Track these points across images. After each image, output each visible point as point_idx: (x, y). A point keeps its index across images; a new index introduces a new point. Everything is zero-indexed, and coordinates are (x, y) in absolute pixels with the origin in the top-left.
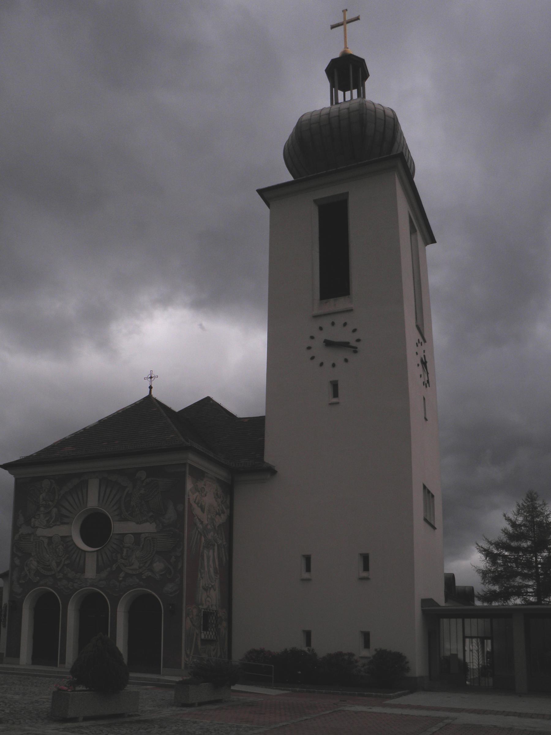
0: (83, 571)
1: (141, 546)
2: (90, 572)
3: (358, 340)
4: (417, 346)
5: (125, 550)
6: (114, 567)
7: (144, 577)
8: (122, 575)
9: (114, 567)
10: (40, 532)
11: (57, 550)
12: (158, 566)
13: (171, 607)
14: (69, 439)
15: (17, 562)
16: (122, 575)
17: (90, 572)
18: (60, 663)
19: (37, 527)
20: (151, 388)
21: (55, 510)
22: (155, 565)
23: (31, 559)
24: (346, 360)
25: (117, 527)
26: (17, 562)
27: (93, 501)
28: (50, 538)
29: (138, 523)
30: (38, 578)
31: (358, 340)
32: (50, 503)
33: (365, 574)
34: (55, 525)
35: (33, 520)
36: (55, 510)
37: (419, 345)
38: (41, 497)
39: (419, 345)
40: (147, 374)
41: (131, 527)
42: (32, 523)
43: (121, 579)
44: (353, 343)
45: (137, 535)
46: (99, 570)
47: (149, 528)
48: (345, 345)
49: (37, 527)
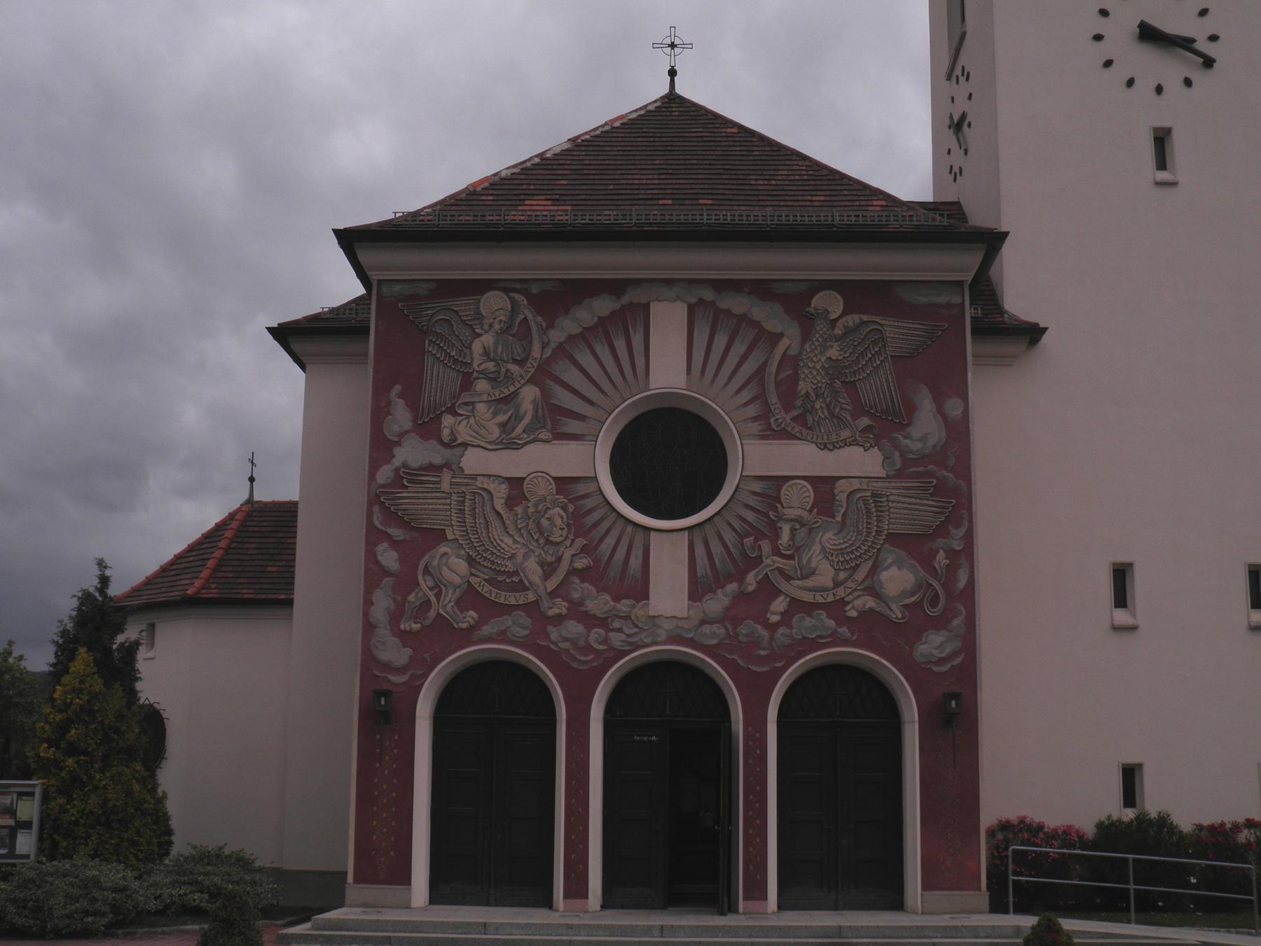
0: (641, 592)
1: (839, 519)
2: (669, 595)
3: (1213, 38)
4: (961, 169)
5: (786, 529)
6: (752, 580)
7: (855, 614)
8: (779, 604)
9: (752, 580)
10: (473, 461)
11: (544, 522)
12: (898, 578)
13: (953, 703)
14: (565, 152)
15: (389, 558)
16: (779, 604)
17: (669, 595)
18: (744, 899)
19: (465, 445)
20: (672, 73)
21: (530, 394)
22: (884, 576)
23: (443, 549)
24: (1188, 82)
25: (751, 457)
26: (389, 558)
27: (668, 367)
28: (516, 483)
29: (824, 447)
30: (472, 613)
31: (1213, 38)
32: (514, 368)
33: (1122, 617)
34: (533, 441)
35: (448, 420)
36: (530, 394)
37: (956, 169)
38: (477, 346)
39: (956, 169)
40: (663, 36)
41: (801, 458)
42: (446, 432)
43: (775, 618)
44: (1202, 45)
45: (823, 486)
46: (697, 591)
47: (859, 463)
48: (1185, 43)
49: (465, 445)
